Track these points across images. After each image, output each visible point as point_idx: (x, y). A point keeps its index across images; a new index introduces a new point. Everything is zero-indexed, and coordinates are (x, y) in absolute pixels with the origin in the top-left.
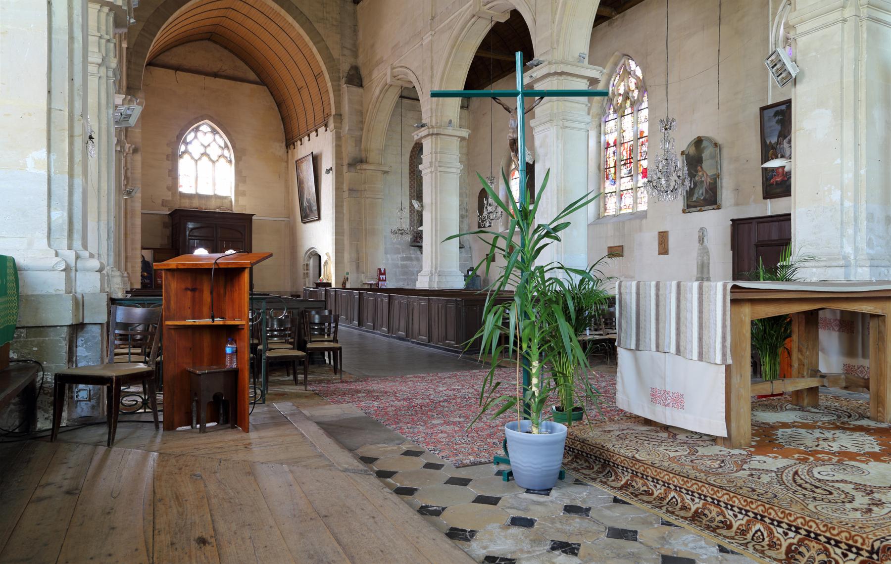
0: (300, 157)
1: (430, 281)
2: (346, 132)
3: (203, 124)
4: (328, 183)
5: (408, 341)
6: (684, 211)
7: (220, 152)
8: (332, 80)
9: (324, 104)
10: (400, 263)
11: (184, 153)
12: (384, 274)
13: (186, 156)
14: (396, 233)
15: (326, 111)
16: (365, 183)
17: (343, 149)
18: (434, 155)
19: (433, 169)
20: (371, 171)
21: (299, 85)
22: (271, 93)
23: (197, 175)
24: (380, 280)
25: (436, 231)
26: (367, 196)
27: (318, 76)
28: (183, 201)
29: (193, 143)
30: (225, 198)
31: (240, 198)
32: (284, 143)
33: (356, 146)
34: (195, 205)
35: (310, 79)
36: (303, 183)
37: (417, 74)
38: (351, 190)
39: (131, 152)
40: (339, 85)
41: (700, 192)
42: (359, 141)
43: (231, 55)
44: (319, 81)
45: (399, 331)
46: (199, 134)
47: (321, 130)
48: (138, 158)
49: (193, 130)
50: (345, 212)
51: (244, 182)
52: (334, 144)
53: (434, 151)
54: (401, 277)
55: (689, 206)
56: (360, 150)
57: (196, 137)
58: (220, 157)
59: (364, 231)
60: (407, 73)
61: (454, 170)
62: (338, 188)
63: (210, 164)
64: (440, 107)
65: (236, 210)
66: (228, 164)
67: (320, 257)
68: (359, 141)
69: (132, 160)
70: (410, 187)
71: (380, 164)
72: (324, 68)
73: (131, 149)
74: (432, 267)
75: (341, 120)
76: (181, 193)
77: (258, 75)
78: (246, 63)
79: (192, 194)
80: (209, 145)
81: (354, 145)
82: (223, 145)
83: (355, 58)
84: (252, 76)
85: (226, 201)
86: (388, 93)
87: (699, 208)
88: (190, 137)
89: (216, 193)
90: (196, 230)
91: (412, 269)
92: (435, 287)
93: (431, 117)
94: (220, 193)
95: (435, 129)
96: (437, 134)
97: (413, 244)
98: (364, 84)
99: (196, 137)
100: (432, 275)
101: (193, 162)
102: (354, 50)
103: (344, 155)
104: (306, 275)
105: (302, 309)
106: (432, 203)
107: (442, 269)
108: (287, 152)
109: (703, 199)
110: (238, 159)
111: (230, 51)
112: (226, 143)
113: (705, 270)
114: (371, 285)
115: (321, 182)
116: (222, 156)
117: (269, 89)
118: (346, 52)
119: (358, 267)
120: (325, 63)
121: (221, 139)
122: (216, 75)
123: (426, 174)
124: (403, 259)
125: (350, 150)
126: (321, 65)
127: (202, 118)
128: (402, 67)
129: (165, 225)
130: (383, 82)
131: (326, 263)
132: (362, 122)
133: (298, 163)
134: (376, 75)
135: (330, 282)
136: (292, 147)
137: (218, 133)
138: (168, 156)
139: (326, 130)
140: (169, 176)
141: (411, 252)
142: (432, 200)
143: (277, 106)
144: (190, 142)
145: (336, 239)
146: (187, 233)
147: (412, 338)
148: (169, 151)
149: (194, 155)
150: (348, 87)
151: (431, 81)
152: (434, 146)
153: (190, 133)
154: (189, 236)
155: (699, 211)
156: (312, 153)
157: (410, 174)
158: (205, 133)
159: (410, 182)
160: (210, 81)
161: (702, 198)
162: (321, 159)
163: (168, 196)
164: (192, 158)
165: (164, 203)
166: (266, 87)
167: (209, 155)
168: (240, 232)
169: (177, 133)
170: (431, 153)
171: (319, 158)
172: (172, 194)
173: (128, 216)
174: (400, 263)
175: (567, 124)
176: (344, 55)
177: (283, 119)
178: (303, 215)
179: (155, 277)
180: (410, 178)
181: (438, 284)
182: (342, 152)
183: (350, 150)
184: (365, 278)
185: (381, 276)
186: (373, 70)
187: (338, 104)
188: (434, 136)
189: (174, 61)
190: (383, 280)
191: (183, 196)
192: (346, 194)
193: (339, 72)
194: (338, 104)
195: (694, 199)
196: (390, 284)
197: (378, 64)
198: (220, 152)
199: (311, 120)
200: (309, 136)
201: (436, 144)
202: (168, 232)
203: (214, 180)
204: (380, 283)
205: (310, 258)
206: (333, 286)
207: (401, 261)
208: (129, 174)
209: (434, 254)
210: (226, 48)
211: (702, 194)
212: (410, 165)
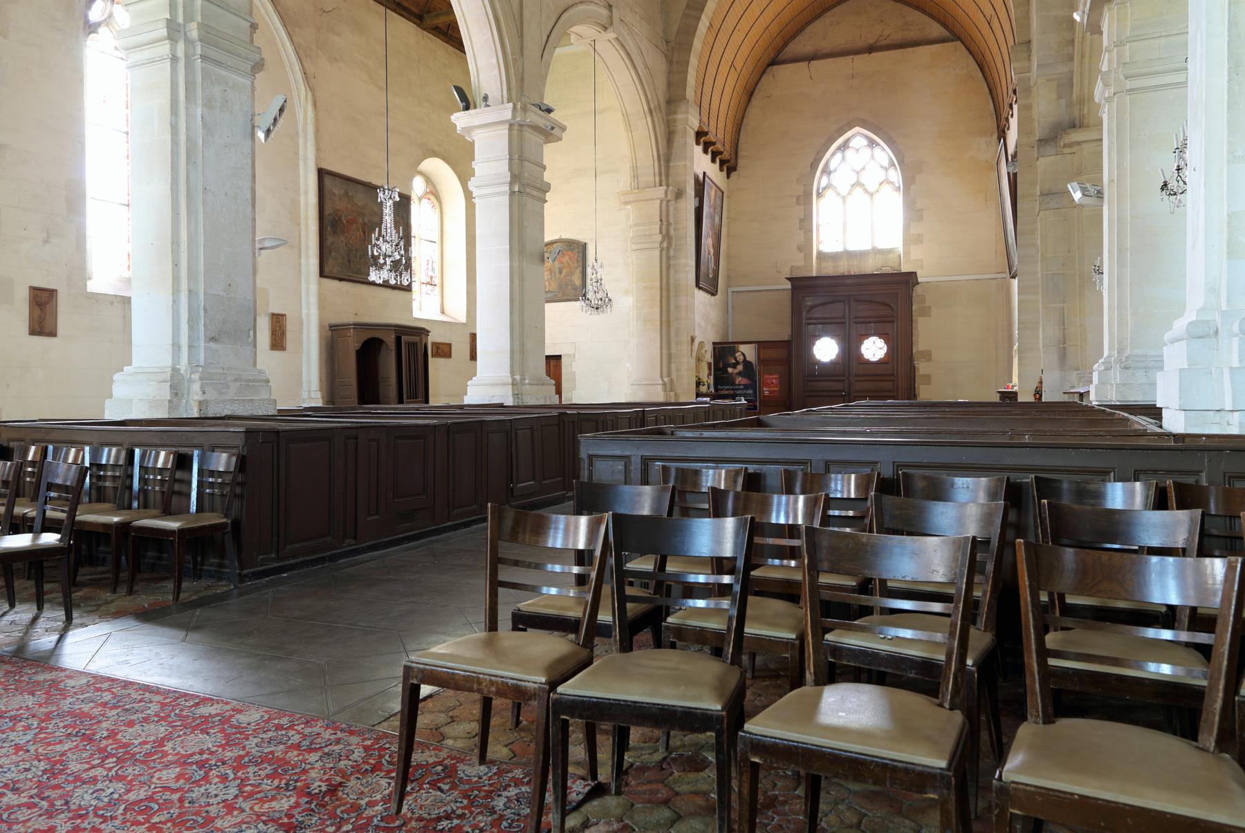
3: (854, 136)
7: (881, 175)
13: (829, 194)
28: (824, 265)
30: (890, 251)
33: (1059, 98)
49: (839, 148)
51: (920, 219)
57: (843, 158)
58: (881, 184)
63: (867, 197)
68: (1065, 86)
76: (820, 254)
78: (923, 11)
80: (864, 169)
81: (1054, 96)
84: (937, 30)
85: (891, 256)
94: (882, 245)
99: (843, 158)
101: (840, 200)
107: (1136, 351)
110: (908, 181)
116: (887, 181)
119: (1063, 357)
121: (884, 154)
122: (871, 49)
127: (850, 126)
137: (878, 145)
138: (798, 198)
140: (800, 229)
146: (804, 314)
149: (839, 190)
153: (833, 155)
158: (858, 150)
164: (866, 191)
166: (959, 42)
167: (863, 185)
169: (811, 160)
179: (760, 387)
198: (881, 175)
208: (672, 232)
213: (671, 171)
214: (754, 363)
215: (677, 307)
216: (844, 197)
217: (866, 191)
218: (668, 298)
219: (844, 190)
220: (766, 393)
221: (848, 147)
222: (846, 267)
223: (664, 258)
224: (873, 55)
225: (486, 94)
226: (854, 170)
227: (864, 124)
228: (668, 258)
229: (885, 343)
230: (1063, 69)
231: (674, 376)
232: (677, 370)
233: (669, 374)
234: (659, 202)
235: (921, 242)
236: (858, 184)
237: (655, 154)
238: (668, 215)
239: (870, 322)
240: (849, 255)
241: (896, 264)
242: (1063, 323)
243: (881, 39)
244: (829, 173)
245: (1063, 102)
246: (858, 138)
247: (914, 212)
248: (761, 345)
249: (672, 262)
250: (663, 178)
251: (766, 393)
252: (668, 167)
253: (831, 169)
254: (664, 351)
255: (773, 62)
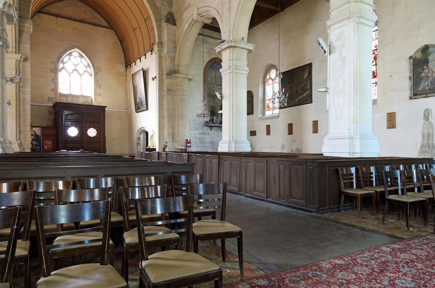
0: (134, 72)
1: (229, 146)
2: (165, 54)
3: (74, 51)
4: (153, 86)
5: (241, 195)
6: (411, 98)
7: (85, 69)
8: (156, 21)
9: (151, 36)
10: (198, 136)
11: (62, 68)
12: (190, 143)
13: (63, 71)
14: (200, 116)
15: (152, 42)
16: (177, 86)
17: (163, 64)
18: (231, 62)
19: (231, 71)
20: (181, 79)
21: (134, 27)
22: (116, 34)
23: (70, 82)
24: (187, 147)
25: (233, 112)
26: (179, 94)
27: (147, 19)
28: (62, 98)
29: (68, 62)
30: (88, 97)
31: (98, 97)
32: (124, 65)
33: (171, 63)
34: (70, 100)
35: (142, 22)
36: (136, 88)
37: (217, 9)
38: (168, 90)
39: (22, 60)
40: (161, 24)
41: (426, 84)
42: (173, 59)
43: (92, 10)
44: (147, 22)
45: (211, 181)
46: (72, 57)
47: (149, 54)
48: (28, 64)
49: (68, 54)
50: (164, 104)
51: (100, 87)
52: (158, 61)
53: (231, 58)
54: (200, 145)
55: (415, 95)
56: (174, 65)
57: (69, 59)
58: (85, 72)
59: (177, 116)
60: (209, 10)
61: (245, 72)
62: (160, 89)
63: (79, 76)
64: (236, 28)
65: (94, 104)
66: (90, 77)
67: (147, 133)
68: (173, 59)
69: (23, 65)
70: (204, 90)
71: (187, 74)
72: (151, 13)
73: (22, 58)
74: (230, 137)
75: (162, 46)
76: (60, 94)
77: (108, 23)
78: (101, 15)
79: (67, 94)
80: (78, 65)
81: (170, 62)
82: (87, 65)
83: (171, 8)
84: (105, 23)
85: (88, 99)
86: (193, 27)
87: (425, 96)
88: (66, 59)
89: (82, 94)
90: (70, 115)
91: (205, 140)
92: (233, 150)
93: (229, 35)
95: (233, 43)
96: (234, 47)
97: (206, 125)
98: (177, 23)
99: (69, 59)
100: (230, 143)
101: (68, 74)
102: (170, 2)
103: (164, 68)
104: (139, 144)
105: (170, 174)
106: (230, 94)
108: (126, 70)
109: (428, 89)
110: (96, 73)
111: (91, 7)
112: (88, 64)
113: (431, 138)
114: (182, 149)
115: (148, 83)
117: (115, 32)
118: (165, 3)
119: (173, 138)
120: (152, 10)
121: (86, 61)
122: (82, 21)
123: (225, 75)
124: (200, 134)
125: (167, 65)
126: (149, 11)
128: (205, 7)
129: (50, 113)
130: (191, 19)
131: (152, 136)
132: (175, 48)
133: (134, 75)
134: (186, 15)
135: (155, 148)
136: (129, 67)
138: (51, 70)
139: (152, 54)
141: (205, 130)
142: (229, 92)
143: (120, 42)
144: (66, 62)
145: (159, 121)
146: (64, 117)
147: (246, 191)
148: (53, 67)
149: (68, 70)
150: (166, 24)
151: (229, 11)
152: (231, 55)
153: (66, 56)
154: (65, 119)
155: (425, 97)
156: (143, 68)
157: (204, 82)
158: (76, 57)
159: (204, 87)
160: (78, 25)
161: (427, 88)
162: (148, 72)
163: (52, 95)
164: (79, 73)
165: (49, 99)
166: (113, 31)
167: (78, 71)
168: (98, 118)
169: (58, 56)
170: (229, 60)
171: (147, 72)
172: (54, 94)
173: (21, 103)
174: (198, 136)
175: (362, 20)
176: (163, 5)
177: (123, 50)
178: (137, 108)
180: (204, 84)
181: (235, 149)
182: (163, 67)
183: (167, 65)
184: (178, 146)
185: (188, 144)
186: (183, 13)
187: (160, 36)
188: (231, 49)
189: (55, 11)
190: (189, 147)
191: (61, 95)
192: (165, 93)
193: (161, 16)
194: (160, 36)
195: (420, 89)
196: (193, 149)
197: (186, 9)
198: (85, 69)
199: (141, 48)
200: (140, 59)
201: (233, 54)
202: (52, 117)
203: (81, 86)
204: (187, 148)
205: (141, 134)
206: (157, 150)
207: (199, 135)
209: (231, 129)
210: (88, 5)
211: (428, 85)
212: (204, 77)
213: (21, 48)
214: (40, 135)
215: (24, 109)
216: (70, 74)
217: (79, 73)
218: (19, 105)
219: (70, 71)
220: (46, 148)
221: (71, 55)
222: (71, 101)
223: (18, 87)
224: (83, 24)
225: (243, 37)
226: (73, 64)
227: (79, 48)
228: (19, 87)
229: (96, 130)
230: (173, 54)
231: (22, 140)
232: (24, 138)
233: (20, 139)
234: (15, 60)
235: (101, 96)
236: (75, 70)
237: (14, 39)
238: (19, 67)
239: (91, 123)
240: (73, 96)
241: (90, 102)
242: (173, 128)
243: (85, 19)
244: (64, 63)
245: (172, 64)
246: (76, 53)
247: (97, 84)
248: (43, 128)
249: (21, 89)
250: (17, 50)
251: (46, 148)
252: (19, 46)
253: (65, 61)
254: (18, 129)
255: (39, 12)
